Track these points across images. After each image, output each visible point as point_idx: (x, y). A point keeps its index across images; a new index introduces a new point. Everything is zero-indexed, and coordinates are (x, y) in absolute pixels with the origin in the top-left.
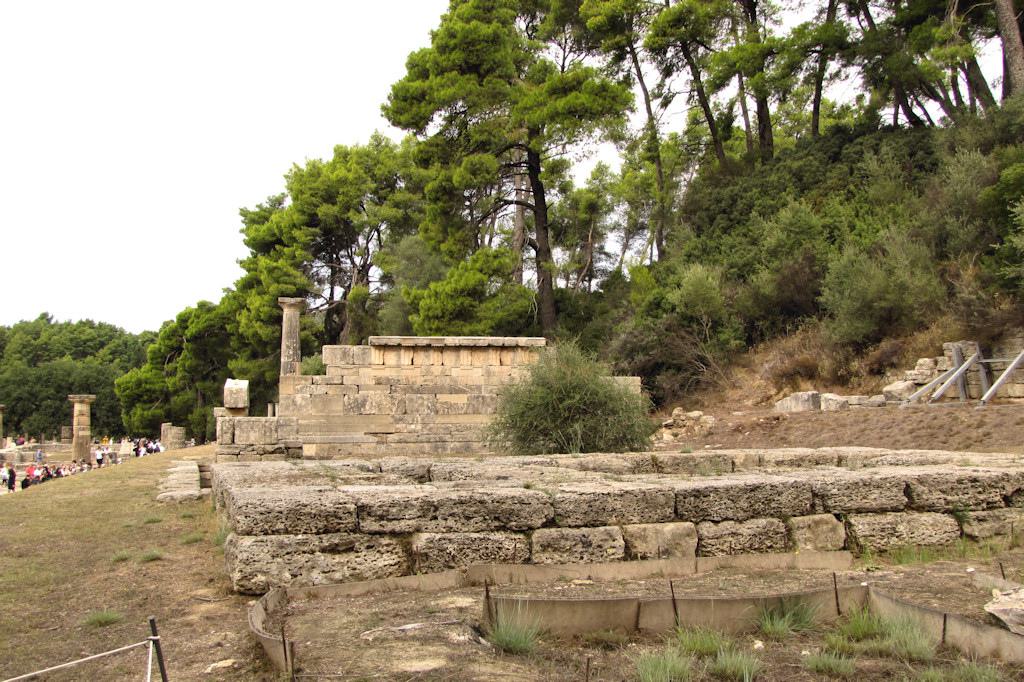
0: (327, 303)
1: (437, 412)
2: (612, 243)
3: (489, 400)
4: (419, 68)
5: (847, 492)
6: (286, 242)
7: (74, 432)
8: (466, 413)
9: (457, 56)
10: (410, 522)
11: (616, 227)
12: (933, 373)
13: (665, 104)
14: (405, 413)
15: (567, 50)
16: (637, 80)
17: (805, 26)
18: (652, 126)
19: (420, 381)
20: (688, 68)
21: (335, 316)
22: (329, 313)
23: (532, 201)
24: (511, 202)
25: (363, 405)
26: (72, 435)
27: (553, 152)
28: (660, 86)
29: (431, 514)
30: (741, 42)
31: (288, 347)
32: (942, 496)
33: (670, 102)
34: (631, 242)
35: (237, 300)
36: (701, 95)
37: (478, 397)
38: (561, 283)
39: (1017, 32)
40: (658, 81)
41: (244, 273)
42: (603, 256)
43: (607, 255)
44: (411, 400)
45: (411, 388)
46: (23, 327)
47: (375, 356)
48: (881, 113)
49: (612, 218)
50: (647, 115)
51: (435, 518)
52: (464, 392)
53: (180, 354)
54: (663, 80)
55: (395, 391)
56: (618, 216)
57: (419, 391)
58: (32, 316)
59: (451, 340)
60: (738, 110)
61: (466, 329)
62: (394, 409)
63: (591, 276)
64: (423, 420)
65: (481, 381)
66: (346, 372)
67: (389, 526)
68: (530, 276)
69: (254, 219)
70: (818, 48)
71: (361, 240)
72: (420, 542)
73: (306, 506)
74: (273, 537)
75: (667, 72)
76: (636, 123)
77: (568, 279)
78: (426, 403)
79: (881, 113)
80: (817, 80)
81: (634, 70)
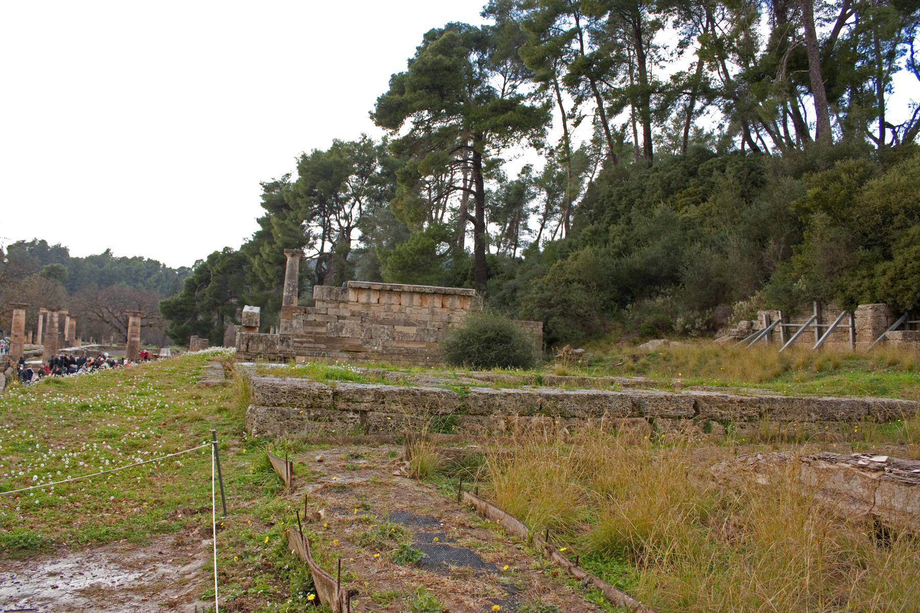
0: (319, 253)
1: (394, 339)
2: (533, 222)
3: (432, 332)
4: (397, 82)
5: (655, 404)
6: (291, 207)
7: (128, 338)
8: (415, 341)
9: (426, 80)
10: (366, 404)
11: (535, 211)
12: (749, 332)
13: (576, 124)
14: (371, 338)
15: (507, 78)
16: (557, 103)
17: (680, 74)
18: (566, 137)
19: (383, 315)
20: (595, 98)
21: (324, 263)
22: (320, 260)
23: (473, 189)
24: (459, 188)
25: (341, 330)
26: (127, 340)
27: (493, 154)
28: (574, 110)
29: (381, 400)
30: (636, 83)
31: (289, 285)
32: (719, 410)
33: (580, 122)
34: (547, 222)
35: (251, 248)
36: (603, 117)
37: (424, 329)
38: (493, 250)
39: (824, 93)
40: (572, 106)
41: (259, 228)
42: (526, 232)
43: (530, 231)
44: (376, 329)
45: (376, 320)
46: (92, 259)
47: (352, 296)
48: (734, 139)
49: (532, 204)
50: (563, 132)
51: (383, 403)
52: (414, 325)
53: (208, 284)
54: (576, 105)
55: (365, 322)
56: (539, 201)
57: (382, 322)
58: (99, 252)
59: (406, 287)
60: (630, 130)
61: (419, 280)
62: (363, 335)
63: (517, 246)
64: (383, 343)
65: (427, 318)
66: (330, 305)
67: (353, 406)
68: (469, 243)
69: (268, 188)
70: (688, 91)
71: (347, 209)
72: (373, 417)
73: (300, 389)
74: (278, 408)
75: (579, 101)
76: (553, 136)
77: (499, 247)
78: (386, 331)
79: (734, 139)
80: (689, 113)
81: (555, 97)
